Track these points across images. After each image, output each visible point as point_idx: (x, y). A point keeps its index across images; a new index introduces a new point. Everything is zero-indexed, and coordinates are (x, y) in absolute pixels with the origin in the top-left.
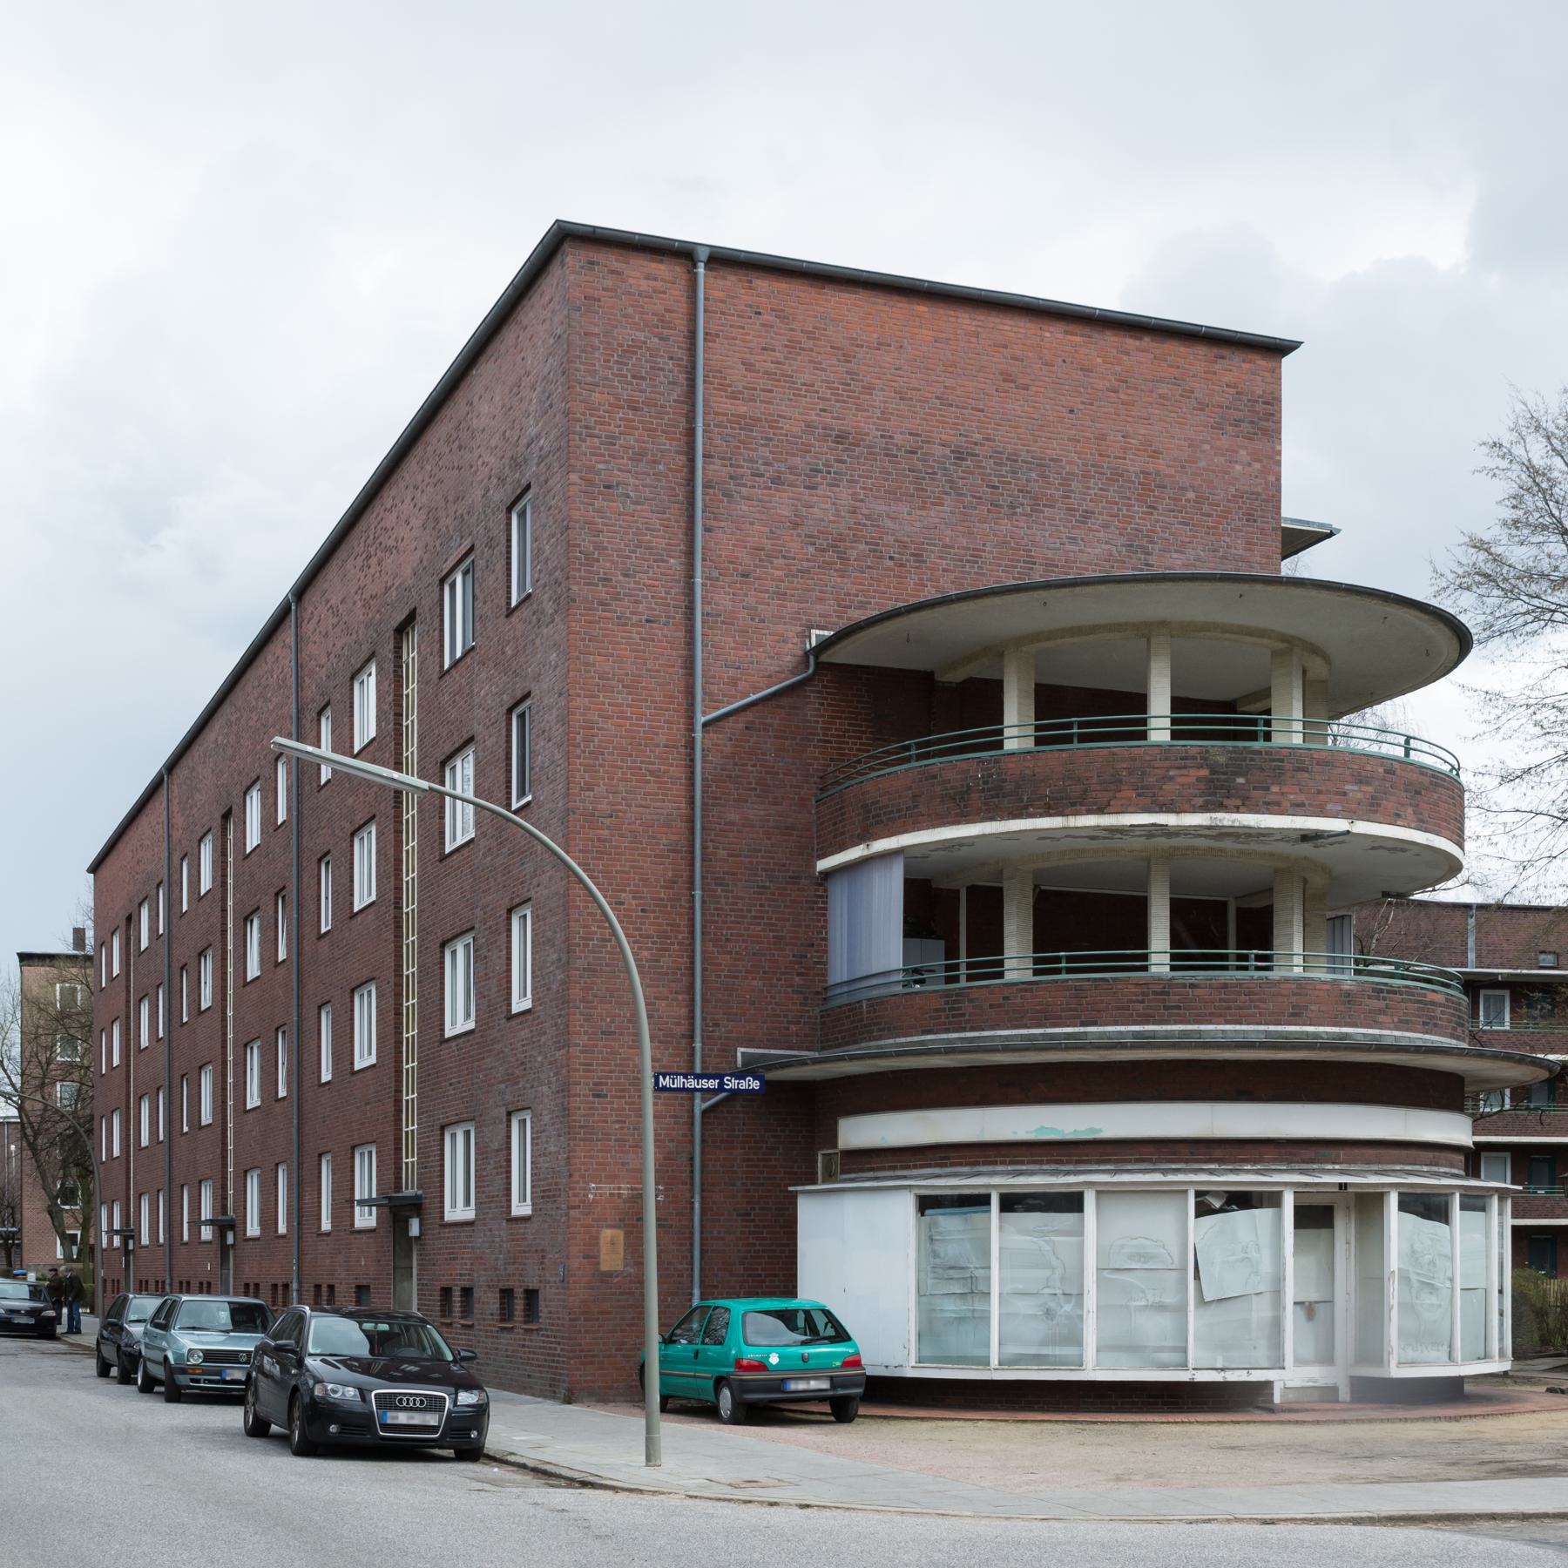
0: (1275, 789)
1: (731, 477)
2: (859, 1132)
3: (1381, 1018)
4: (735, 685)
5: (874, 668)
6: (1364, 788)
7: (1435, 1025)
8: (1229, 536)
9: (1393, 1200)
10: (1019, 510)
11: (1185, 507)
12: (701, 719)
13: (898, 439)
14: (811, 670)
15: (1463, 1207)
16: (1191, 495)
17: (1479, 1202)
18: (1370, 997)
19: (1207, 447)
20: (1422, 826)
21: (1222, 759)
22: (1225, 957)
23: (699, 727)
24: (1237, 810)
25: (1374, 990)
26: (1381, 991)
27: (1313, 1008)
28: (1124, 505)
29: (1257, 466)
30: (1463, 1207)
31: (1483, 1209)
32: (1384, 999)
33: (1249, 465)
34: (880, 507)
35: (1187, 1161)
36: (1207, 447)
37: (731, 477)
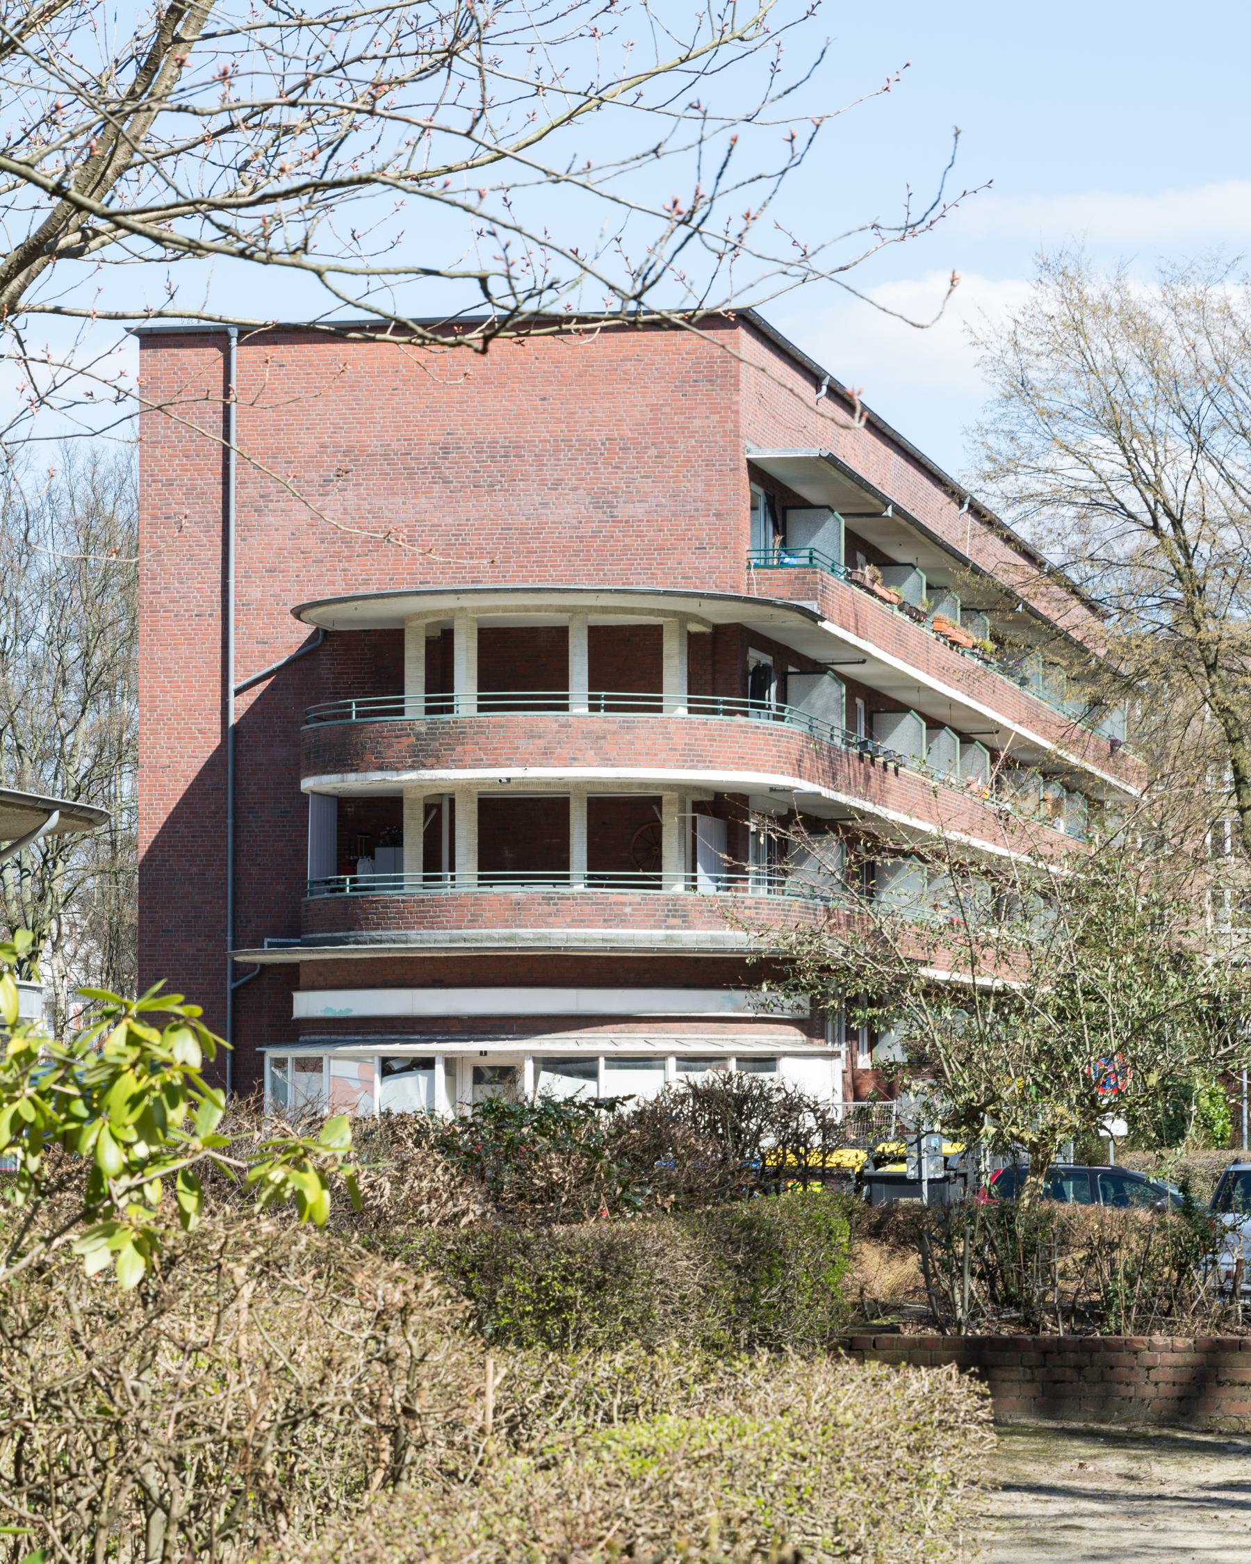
0: (459, 748)
1: (262, 497)
2: (307, 1004)
3: (550, 920)
4: (264, 657)
5: (375, 631)
6: (537, 741)
7: (622, 921)
8: (689, 481)
9: (602, 1061)
10: (497, 488)
11: (646, 463)
12: (233, 686)
13: (394, 445)
14: (319, 641)
15: (607, 1067)
16: (653, 452)
17: (587, 1066)
18: (539, 904)
19: (667, 409)
20: (606, 761)
21: (423, 729)
22: (439, 878)
23: (232, 694)
24: (432, 767)
25: (543, 898)
26: (552, 898)
27: (487, 914)
28: (591, 469)
29: (716, 417)
30: (607, 1067)
31: (663, 1068)
32: (555, 904)
33: (707, 417)
34: (380, 502)
35: (401, 1033)
36: (667, 409)
37: (262, 497)
